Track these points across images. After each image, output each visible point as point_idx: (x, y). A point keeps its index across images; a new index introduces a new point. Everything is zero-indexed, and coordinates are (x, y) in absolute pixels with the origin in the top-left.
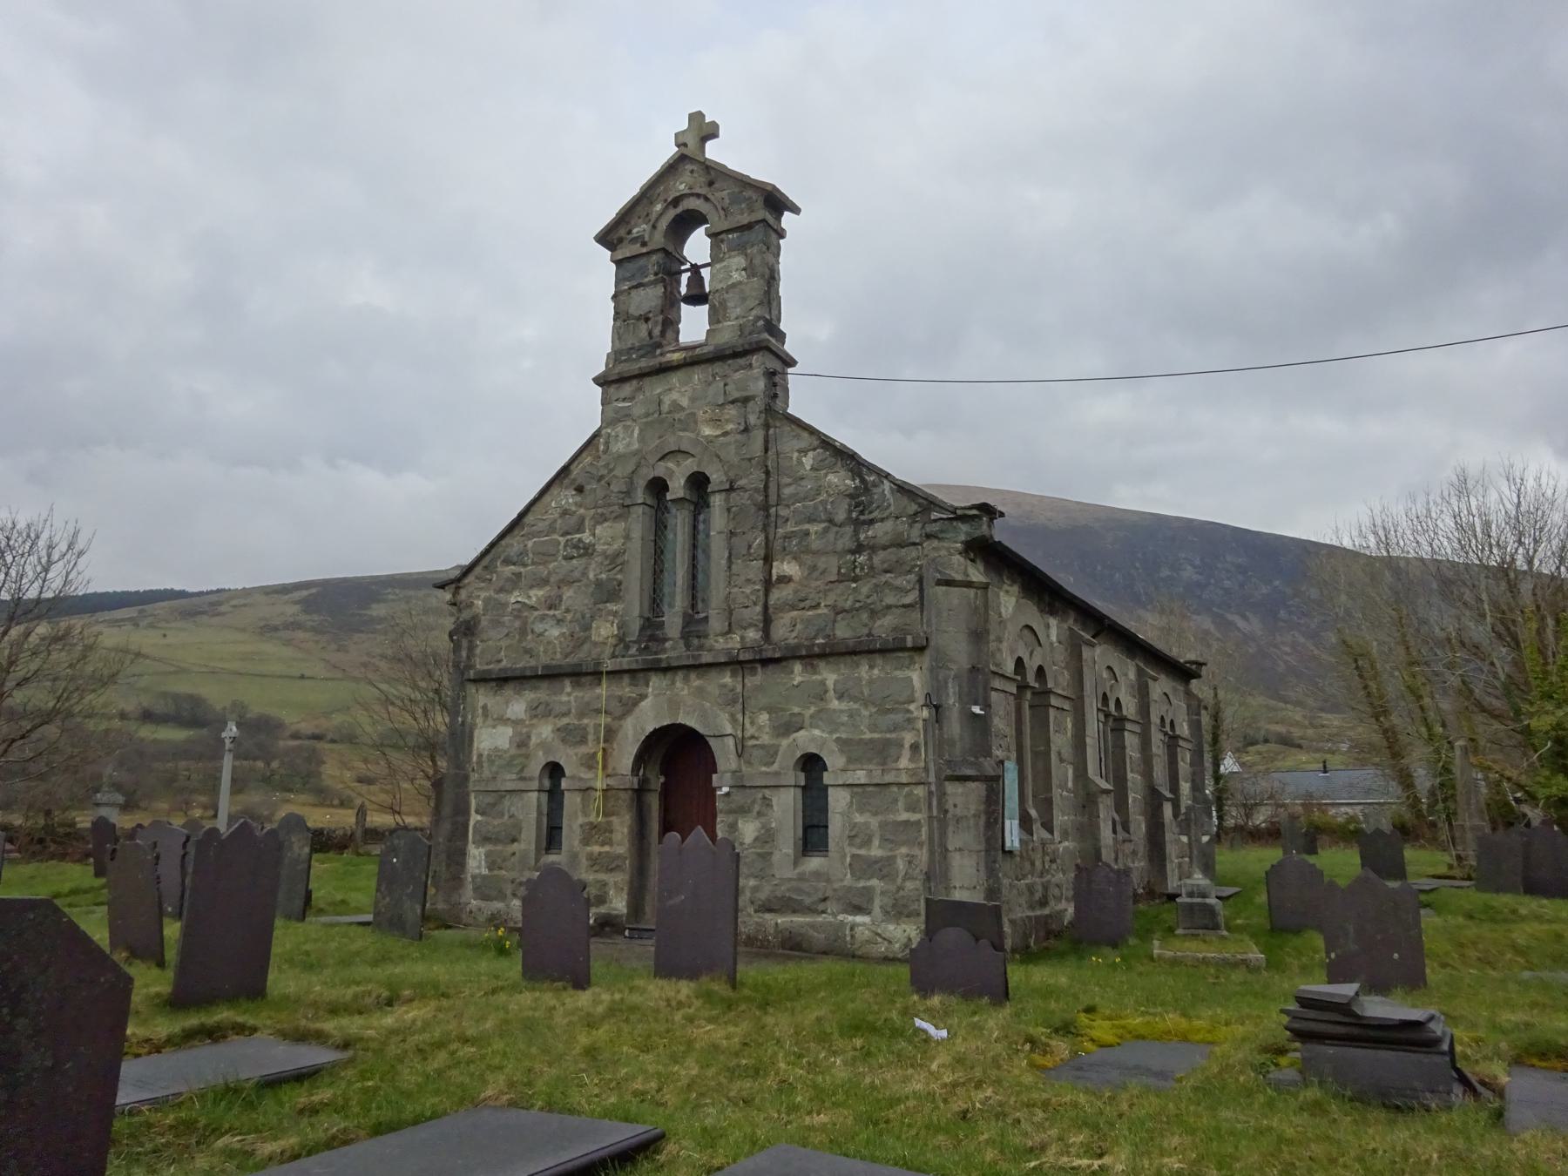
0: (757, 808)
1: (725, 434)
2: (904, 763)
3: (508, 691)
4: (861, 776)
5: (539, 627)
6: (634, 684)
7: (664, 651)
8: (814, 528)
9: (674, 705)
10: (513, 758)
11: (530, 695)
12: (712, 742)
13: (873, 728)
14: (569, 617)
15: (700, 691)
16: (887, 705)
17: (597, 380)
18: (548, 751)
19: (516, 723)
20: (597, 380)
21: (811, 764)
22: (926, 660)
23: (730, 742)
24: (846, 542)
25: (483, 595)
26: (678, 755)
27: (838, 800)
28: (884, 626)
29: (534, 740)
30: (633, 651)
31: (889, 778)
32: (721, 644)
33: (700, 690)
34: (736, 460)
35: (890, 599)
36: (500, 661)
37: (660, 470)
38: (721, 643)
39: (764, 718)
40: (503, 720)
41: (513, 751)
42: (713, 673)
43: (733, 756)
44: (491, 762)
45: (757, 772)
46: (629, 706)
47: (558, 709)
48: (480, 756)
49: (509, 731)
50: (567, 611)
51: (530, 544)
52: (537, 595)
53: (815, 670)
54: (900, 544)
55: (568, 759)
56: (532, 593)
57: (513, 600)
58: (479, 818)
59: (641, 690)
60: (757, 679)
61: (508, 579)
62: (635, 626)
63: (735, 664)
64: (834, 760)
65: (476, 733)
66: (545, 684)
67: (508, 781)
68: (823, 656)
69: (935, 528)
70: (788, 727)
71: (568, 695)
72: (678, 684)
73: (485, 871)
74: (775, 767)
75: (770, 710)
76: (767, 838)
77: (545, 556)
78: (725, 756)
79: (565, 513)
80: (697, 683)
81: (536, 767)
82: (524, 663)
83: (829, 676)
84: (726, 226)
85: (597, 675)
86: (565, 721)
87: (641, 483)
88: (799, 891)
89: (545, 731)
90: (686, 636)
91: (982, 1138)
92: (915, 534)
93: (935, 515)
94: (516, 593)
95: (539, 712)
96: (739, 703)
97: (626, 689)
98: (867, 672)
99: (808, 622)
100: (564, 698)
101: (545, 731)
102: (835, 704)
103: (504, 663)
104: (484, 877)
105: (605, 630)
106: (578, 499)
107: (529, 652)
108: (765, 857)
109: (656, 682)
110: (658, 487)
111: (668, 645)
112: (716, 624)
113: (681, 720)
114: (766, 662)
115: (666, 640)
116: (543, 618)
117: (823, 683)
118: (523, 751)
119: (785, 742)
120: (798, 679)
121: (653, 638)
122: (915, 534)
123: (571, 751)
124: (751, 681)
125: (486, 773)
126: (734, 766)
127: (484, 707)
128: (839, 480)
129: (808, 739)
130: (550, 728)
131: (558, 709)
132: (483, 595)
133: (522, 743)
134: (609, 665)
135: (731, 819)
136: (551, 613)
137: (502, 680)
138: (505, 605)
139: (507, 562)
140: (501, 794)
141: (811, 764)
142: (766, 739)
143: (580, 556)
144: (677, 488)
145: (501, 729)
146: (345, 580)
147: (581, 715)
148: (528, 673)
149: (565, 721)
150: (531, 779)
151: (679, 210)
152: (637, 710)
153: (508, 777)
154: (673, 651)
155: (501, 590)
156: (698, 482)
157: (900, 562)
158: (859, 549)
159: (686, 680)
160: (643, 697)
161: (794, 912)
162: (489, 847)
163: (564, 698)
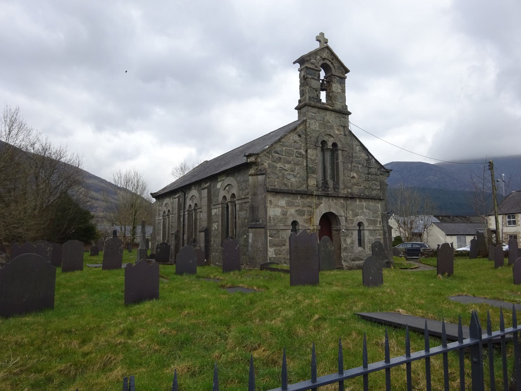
0: (350, 235)
1: (341, 134)
2: (378, 225)
3: (279, 196)
4: (371, 228)
5: (289, 177)
6: (319, 199)
7: (329, 191)
8: (360, 166)
9: (330, 207)
10: (282, 218)
11: (286, 199)
12: (339, 217)
13: (373, 217)
14: (298, 176)
15: (336, 203)
16: (375, 212)
17: (296, 109)
18: (293, 217)
19: (282, 207)
20: (296, 109)
21: (360, 224)
22: (383, 203)
23: (344, 218)
24: (366, 171)
25: (267, 162)
26: (328, 221)
27: (367, 233)
28: (374, 193)
29: (289, 213)
30: (320, 190)
31: (377, 228)
32: (343, 192)
33: (336, 203)
34: (344, 143)
35: (375, 187)
36: (275, 186)
37: (326, 138)
38: (342, 192)
39: (351, 212)
40: (277, 206)
41: (281, 216)
42: (339, 199)
43: (344, 222)
44: (274, 220)
45: (350, 226)
46: (317, 205)
47: (296, 204)
48: (270, 217)
49: (280, 210)
50: (298, 173)
51: (284, 148)
52: (287, 166)
53: (362, 202)
54: (376, 175)
55: (300, 220)
56: (286, 165)
57: (279, 166)
58: (271, 238)
59: (320, 201)
60: (349, 202)
61: (277, 159)
62: (321, 182)
63: (346, 198)
64: (366, 224)
65: (268, 209)
66: (292, 196)
67: (281, 226)
68: (363, 198)
69: (382, 172)
70: (356, 215)
71: (299, 200)
72: (331, 201)
73: (274, 256)
74: (354, 225)
75: (352, 210)
76: (352, 243)
77: (290, 154)
78: (342, 220)
79: (295, 142)
80: (335, 201)
81: (290, 222)
82: (283, 188)
83: (364, 204)
84: (338, 75)
85: (312, 195)
86: (298, 208)
87: (320, 141)
88: (360, 255)
89: (292, 211)
90: (334, 188)
91: (455, 344)
92: (379, 173)
93: (382, 170)
94: (280, 164)
95: (290, 204)
96: (345, 208)
97: (315, 201)
98: (371, 203)
99: (359, 189)
100: (298, 201)
101: (292, 211)
102: (365, 210)
103: (277, 187)
104: (274, 258)
105: (312, 182)
106: (299, 139)
107: (286, 185)
108: (352, 247)
109: (324, 200)
110: (324, 143)
111: (330, 189)
112: (341, 186)
113: (332, 211)
114: (351, 198)
115: (329, 188)
116: (290, 174)
117: (363, 205)
118: (285, 217)
119: (355, 219)
120: (358, 203)
121: (325, 187)
122: (379, 173)
123: (301, 218)
124: (348, 202)
125: (272, 223)
126: (345, 224)
127: (270, 201)
128: (363, 155)
129: (360, 218)
130: (294, 210)
131: (296, 204)
132: (267, 162)
133: (284, 214)
134: (315, 193)
135: (344, 238)
136: (292, 173)
137: (276, 192)
138: (276, 167)
139: (276, 152)
140: (278, 231)
141: (360, 224)
142: (351, 218)
143: (300, 157)
144: (330, 145)
145: (277, 209)
146: (201, 165)
147: (303, 206)
148: (290, 192)
149: (298, 208)
150: (289, 226)
151: (324, 62)
152: (319, 207)
153: (281, 225)
154: (331, 191)
155: (274, 162)
156: (335, 145)
157: (377, 179)
158: (369, 174)
159: (332, 200)
160: (321, 203)
161: (358, 260)
162: (275, 248)
163: (298, 201)
